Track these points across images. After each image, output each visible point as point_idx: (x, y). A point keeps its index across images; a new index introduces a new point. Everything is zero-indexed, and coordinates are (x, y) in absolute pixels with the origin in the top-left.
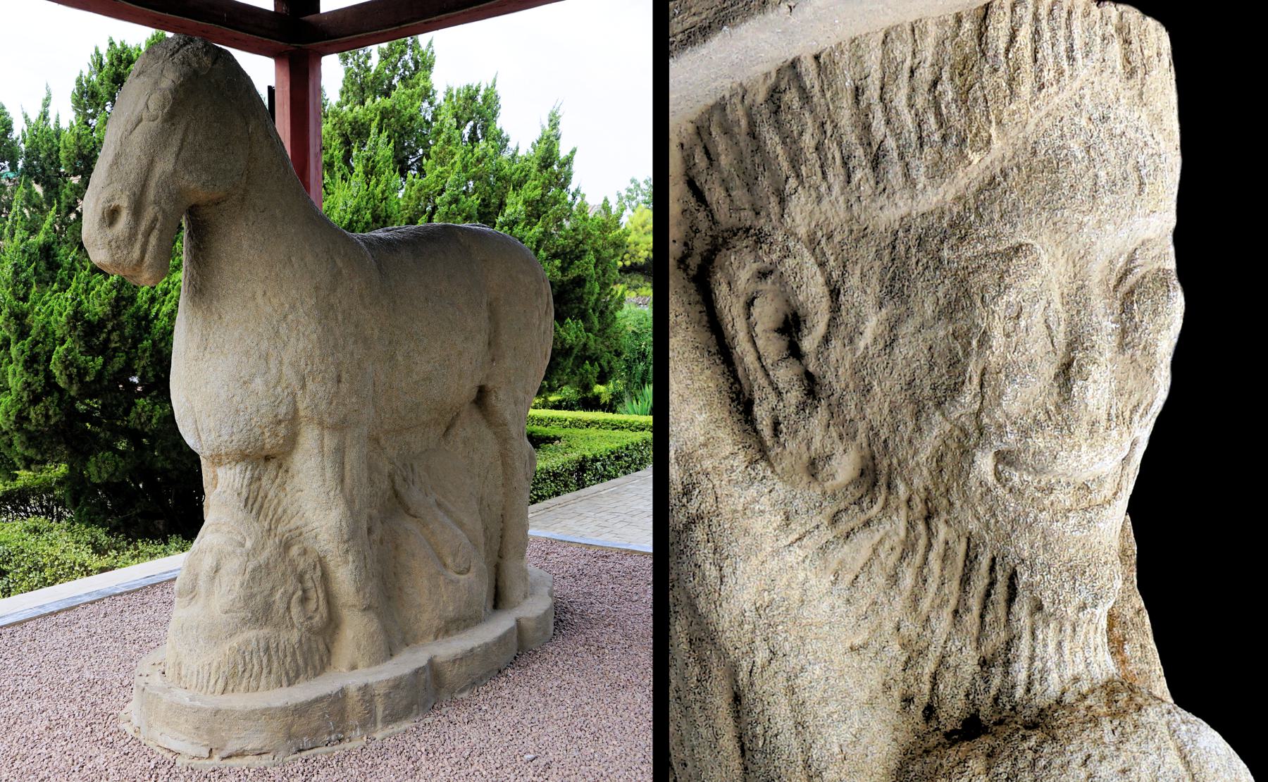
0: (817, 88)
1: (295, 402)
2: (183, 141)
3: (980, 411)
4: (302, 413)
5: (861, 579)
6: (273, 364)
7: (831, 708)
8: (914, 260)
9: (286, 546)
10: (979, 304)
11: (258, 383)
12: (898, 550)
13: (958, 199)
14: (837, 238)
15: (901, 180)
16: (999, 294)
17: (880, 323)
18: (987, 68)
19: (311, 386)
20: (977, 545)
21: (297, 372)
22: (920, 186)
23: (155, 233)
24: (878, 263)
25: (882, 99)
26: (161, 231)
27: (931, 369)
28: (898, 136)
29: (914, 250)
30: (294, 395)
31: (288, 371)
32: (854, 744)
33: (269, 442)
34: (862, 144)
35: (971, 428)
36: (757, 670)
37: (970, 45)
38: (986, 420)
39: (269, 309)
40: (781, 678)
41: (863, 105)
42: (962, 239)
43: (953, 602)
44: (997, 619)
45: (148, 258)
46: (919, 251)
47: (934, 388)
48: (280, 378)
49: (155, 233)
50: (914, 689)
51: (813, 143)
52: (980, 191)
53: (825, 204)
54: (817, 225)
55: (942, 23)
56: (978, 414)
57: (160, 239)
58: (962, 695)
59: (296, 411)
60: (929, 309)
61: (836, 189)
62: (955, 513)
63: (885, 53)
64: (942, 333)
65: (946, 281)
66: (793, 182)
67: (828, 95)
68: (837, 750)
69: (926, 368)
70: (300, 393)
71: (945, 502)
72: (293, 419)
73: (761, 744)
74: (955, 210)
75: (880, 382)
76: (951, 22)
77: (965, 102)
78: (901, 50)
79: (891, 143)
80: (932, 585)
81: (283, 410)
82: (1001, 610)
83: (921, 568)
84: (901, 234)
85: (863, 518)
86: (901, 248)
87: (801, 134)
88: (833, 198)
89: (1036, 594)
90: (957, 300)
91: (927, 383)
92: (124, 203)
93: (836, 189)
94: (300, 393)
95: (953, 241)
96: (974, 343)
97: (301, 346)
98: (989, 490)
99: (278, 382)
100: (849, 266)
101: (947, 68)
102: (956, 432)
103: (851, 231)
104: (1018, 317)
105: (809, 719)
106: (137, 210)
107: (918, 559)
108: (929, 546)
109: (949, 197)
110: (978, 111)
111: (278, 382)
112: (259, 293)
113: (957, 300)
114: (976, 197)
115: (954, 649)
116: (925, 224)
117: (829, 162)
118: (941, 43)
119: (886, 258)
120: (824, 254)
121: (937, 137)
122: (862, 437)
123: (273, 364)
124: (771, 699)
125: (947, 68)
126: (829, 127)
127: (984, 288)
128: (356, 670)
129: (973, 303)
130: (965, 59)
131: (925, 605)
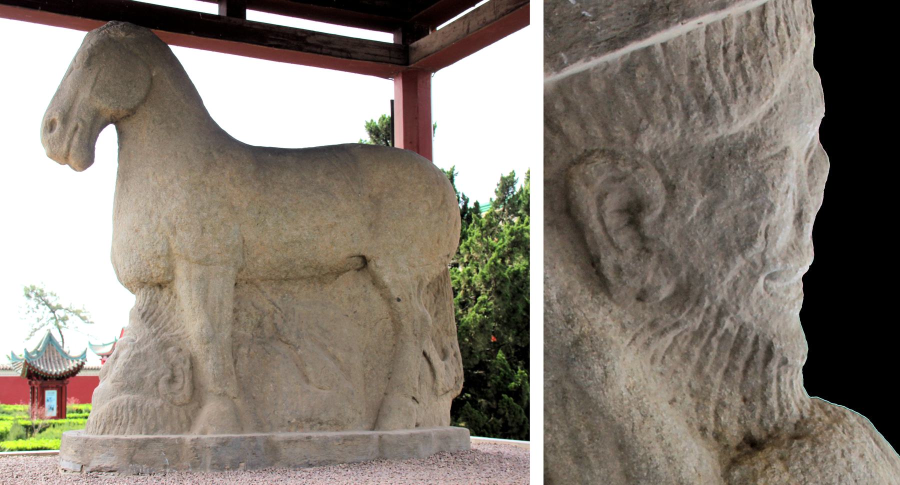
0: (664, 64)
1: (169, 245)
2: (96, 79)
3: (765, 251)
4: (174, 252)
5: (667, 357)
6: (154, 218)
7: (683, 445)
8: (727, 165)
9: (165, 345)
10: (771, 188)
11: (144, 231)
12: (690, 338)
13: (752, 124)
14: (672, 153)
15: (723, 117)
16: (782, 180)
17: (702, 204)
18: (769, 45)
19: (180, 233)
20: (747, 330)
21: (169, 224)
22: (735, 121)
23: (77, 135)
24: (700, 167)
25: (709, 68)
26: (81, 134)
27: (736, 229)
28: (720, 91)
29: (727, 159)
30: (168, 239)
31: (163, 222)
32: (700, 464)
33: (156, 272)
34: (696, 97)
35: (758, 262)
36: (637, 428)
37: (757, 31)
38: (768, 256)
39: (155, 183)
40: (653, 431)
41: (698, 72)
42: (758, 148)
43: (725, 365)
44: (756, 372)
45: (72, 151)
46: (730, 159)
47: (738, 241)
48: (158, 227)
49: (77, 135)
50: (705, 422)
51: (661, 97)
52: (764, 118)
53: (666, 134)
54: (657, 147)
55: (739, 17)
56: (763, 254)
57: (80, 139)
58: (736, 423)
59: (170, 250)
60: (738, 193)
61: (677, 126)
62: (739, 313)
63: (708, 40)
64: (744, 207)
65: (751, 177)
66: (645, 122)
67: (673, 67)
68: (693, 470)
69: (732, 229)
70: (171, 237)
71: (734, 307)
72: (169, 254)
73: (645, 474)
74: (750, 131)
75: (700, 241)
76: (744, 17)
77: (759, 66)
78: (718, 38)
79: (716, 95)
80: (713, 354)
81: (159, 248)
82: (759, 367)
83: (705, 347)
84: (717, 149)
85: (674, 321)
86: (718, 158)
87: (653, 92)
88: (673, 131)
89: (784, 355)
90: (758, 187)
91: (734, 237)
92: (56, 117)
93: (677, 126)
94: (171, 237)
95: (752, 151)
96: (766, 211)
97: (173, 207)
98: (761, 297)
99: (156, 230)
100: (681, 171)
101: (745, 46)
102: (749, 266)
103: (681, 149)
104: (787, 192)
105: (675, 454)
106: (65, 120)
107: (704, 342)
108: (714, 333)
109: (747, 124)
110: (767, 70)
111: (156, 230)
112: (151, 174)
113: (758, 187)
114: (762, 124)
115: (726, 393)
116: (732, 142)
117: (673, 109)
118: (740, 30)
119: (706, 165)
120: (662, 164)
121: (744, 89)
122: (683, 273)
123: (154, 218)
124: (650, 446)
125: (745, 46)
126: (673, 88)
127: (774, 178)
128: (209, 427)
129: (768, 189)
130: (756, 40)
131: (707, 369)
